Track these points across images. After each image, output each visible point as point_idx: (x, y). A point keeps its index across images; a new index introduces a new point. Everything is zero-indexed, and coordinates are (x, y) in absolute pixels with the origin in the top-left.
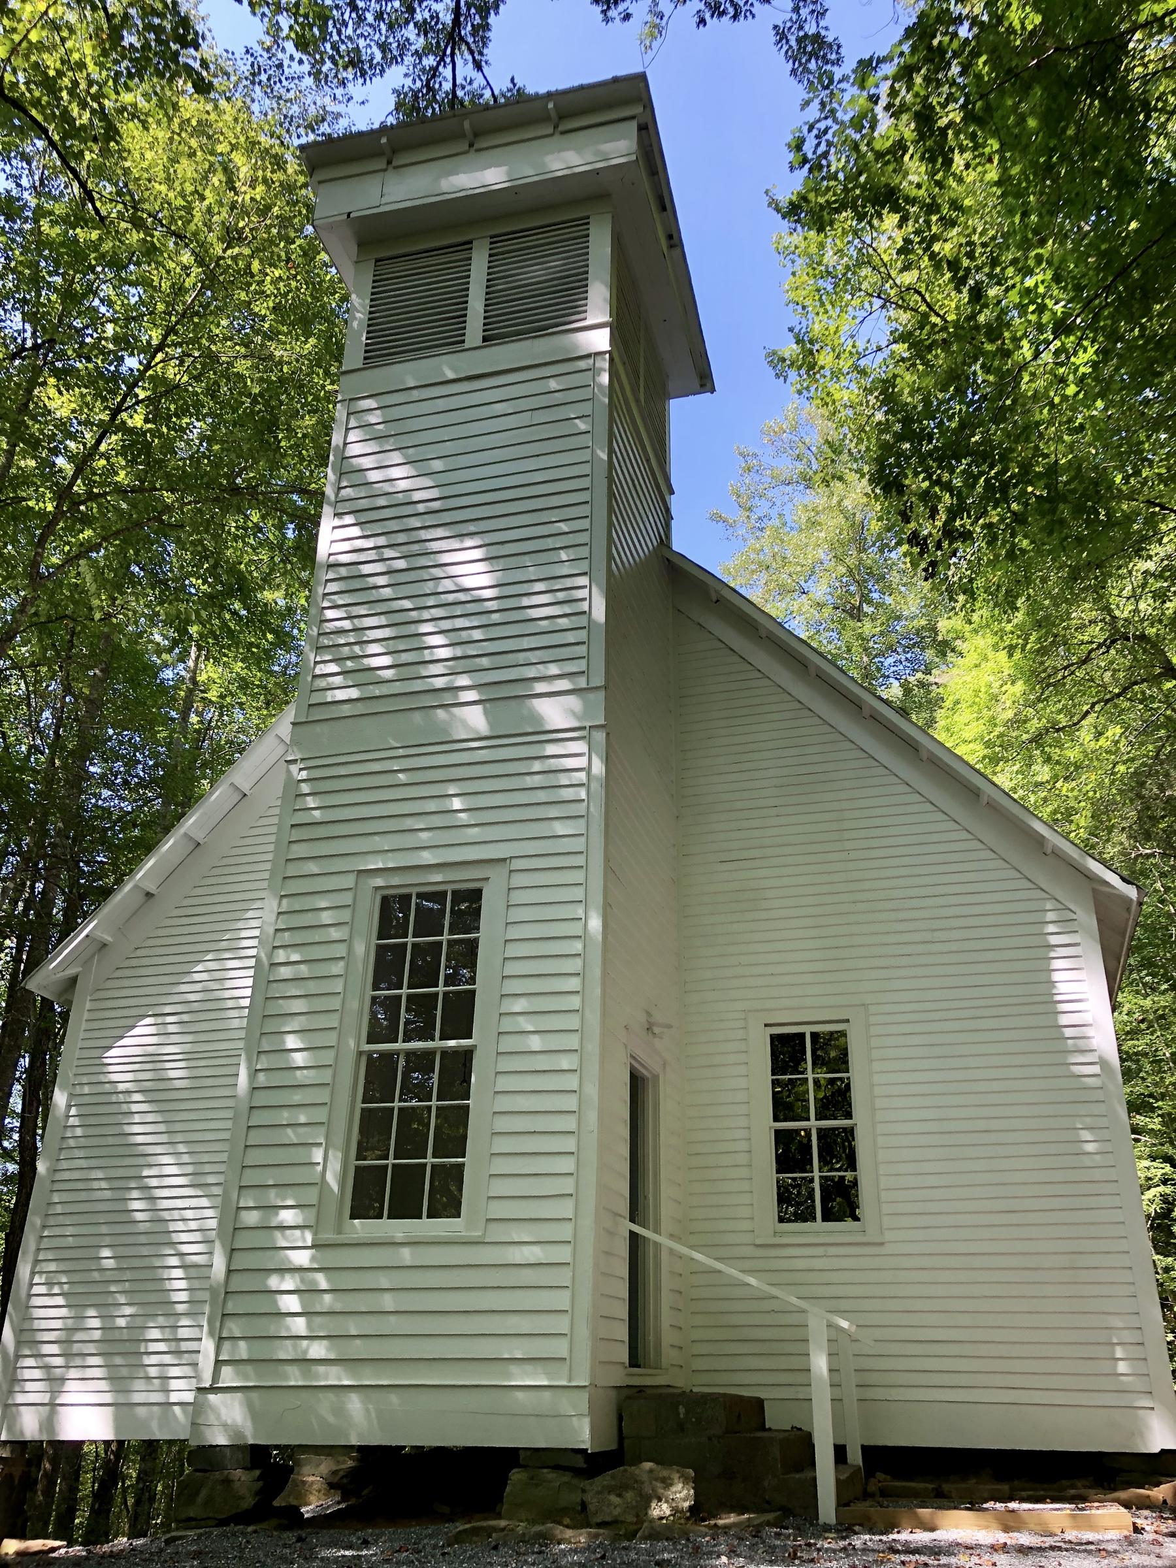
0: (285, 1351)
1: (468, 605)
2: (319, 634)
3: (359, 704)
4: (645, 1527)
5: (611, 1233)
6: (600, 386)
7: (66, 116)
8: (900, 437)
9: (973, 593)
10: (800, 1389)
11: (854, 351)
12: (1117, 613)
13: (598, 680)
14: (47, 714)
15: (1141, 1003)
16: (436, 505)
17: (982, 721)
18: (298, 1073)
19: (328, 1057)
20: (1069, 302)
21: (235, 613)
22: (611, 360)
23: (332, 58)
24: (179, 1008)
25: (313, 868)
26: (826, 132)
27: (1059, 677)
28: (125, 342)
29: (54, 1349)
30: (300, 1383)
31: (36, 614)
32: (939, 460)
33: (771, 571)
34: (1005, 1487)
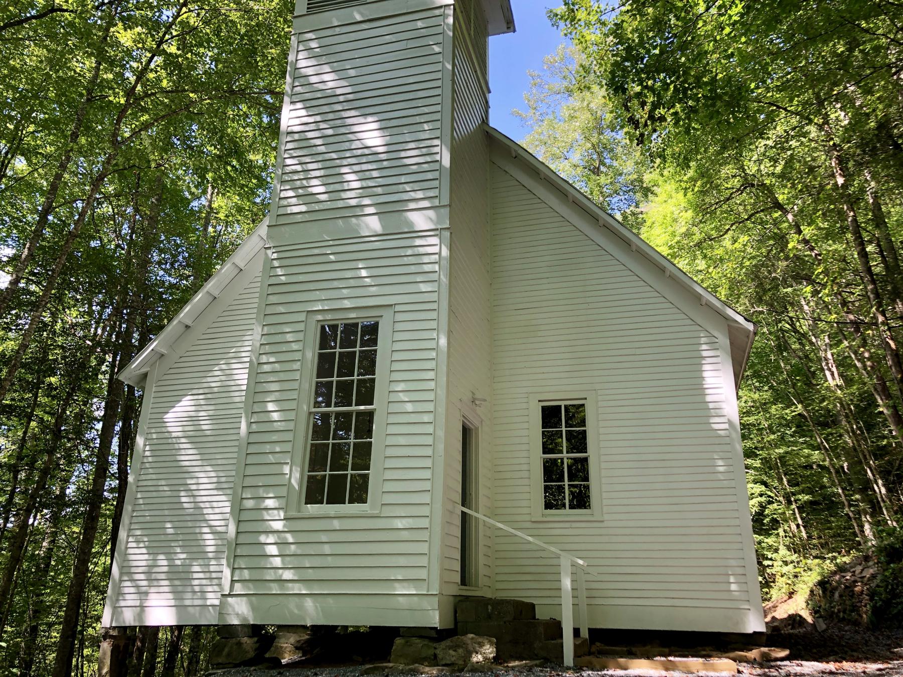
0: (270, 575)
1: (370, 157)
2: (283, 174)
3: (306, 215)
4: (469, 667)
5: (451, 512)
6: (448, 25)
9: (665, 158)
10: (556, 599)
11: (599, 10)
12: (748, 171)
13: (446, 201)
15: (752, 396)
16: (351, 97)
17: (667, 234)
18: (275, 424)
19: (292, 415)
22: (454, 9)
25: (281, 309)
27: (713, 208)
29: (142, 577)
30: (278, 592)
31: (116, 165)
33: (547, 145)
34: (666, 650)
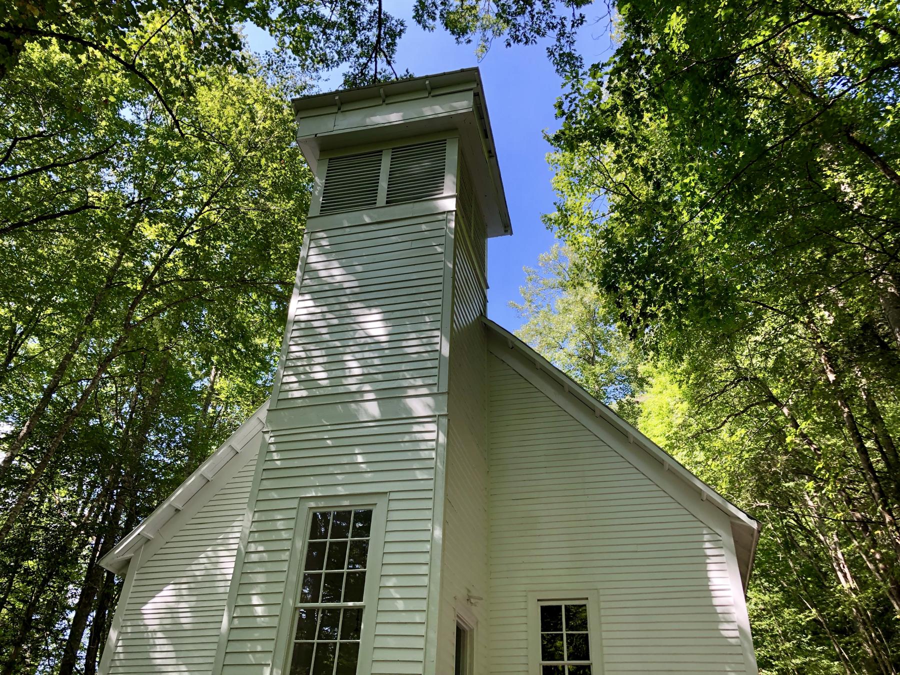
3: (307, 400)
6: (450, 228)
7: (168, 83)
8: (616, 260)
9: (658, 351)
12: (740, 365)
13: (444, 389)
14: (126, 405)
15: (762, 597)
18: (258, 619)
19: (276, 610)
20: (708, 191)
21: (239, 350)
22: (456, 215)
23: (311, 58)
24: (189, 580)
25: (274, 495)
26: (574, 100)
28: (189, 200)
32: (638, 274)
